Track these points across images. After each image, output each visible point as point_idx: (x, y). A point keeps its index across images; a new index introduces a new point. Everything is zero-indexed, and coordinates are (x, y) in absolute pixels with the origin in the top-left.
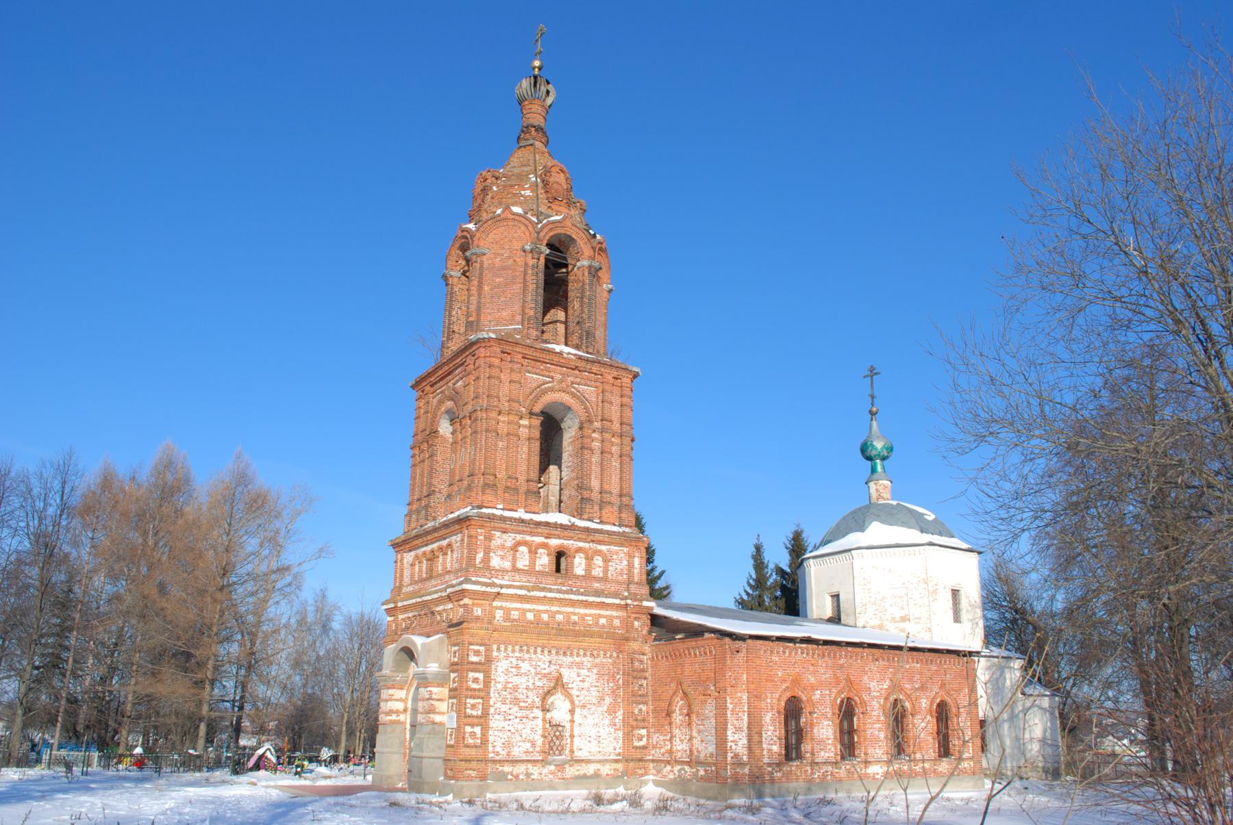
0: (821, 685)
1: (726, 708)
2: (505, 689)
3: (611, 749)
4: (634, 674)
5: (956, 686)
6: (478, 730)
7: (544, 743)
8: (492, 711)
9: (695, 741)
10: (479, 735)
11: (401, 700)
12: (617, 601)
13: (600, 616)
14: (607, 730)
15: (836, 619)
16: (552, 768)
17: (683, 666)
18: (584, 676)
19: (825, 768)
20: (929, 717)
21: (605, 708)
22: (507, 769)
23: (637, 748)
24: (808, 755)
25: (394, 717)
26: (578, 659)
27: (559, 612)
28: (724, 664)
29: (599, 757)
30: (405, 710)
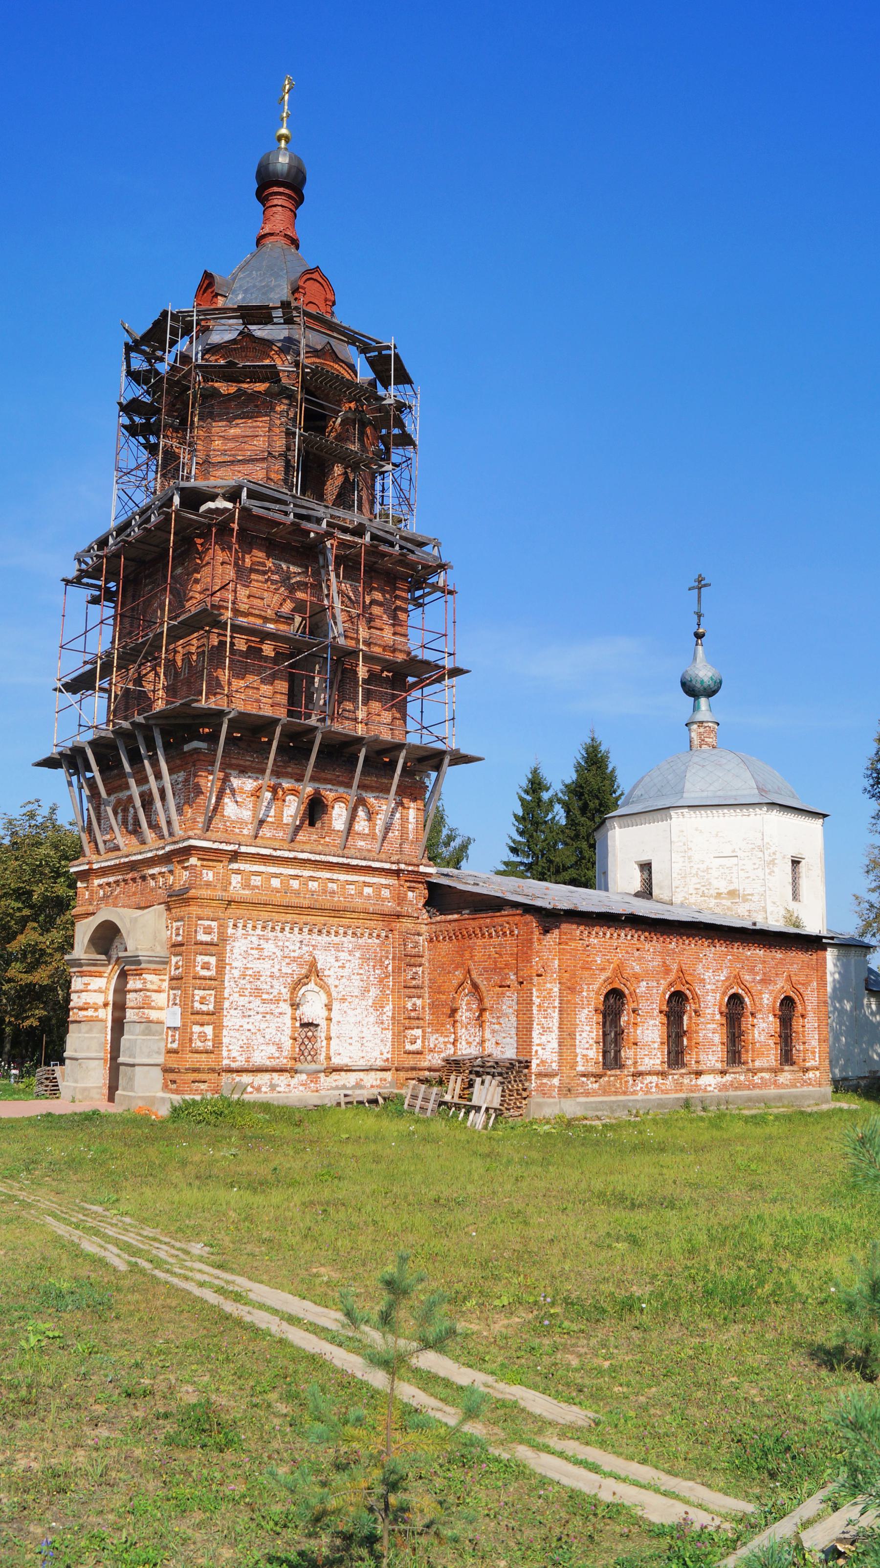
0: (647, 975)
1: (531, 1003)
2: (243, 976)
3: (376, 1054)
4: (410, 960)
5: (802, 978)
6: (209, 1030)
7: (293, 1047)
8: (226, 1004)
9: (487, 1044)
10: (210, 1037)
11: (99, 991)
12: (387, 866)
13: (366, 884)
14: (372, 1029)
15: (647, 892)
16: (304, 1077)
17: (472, 948)
18: (346, 959)
19: (649, 1078)
20: (771, 1018)
21: (370, 1002)
22: (246, 1078)
23: (409, 1053)
24: (629, 1062)
25: (90, 1013)
26: (336, 940)
27: (312, 879)
28: (530, 948)
29: (362, 1063)
30: (106, 1005)
